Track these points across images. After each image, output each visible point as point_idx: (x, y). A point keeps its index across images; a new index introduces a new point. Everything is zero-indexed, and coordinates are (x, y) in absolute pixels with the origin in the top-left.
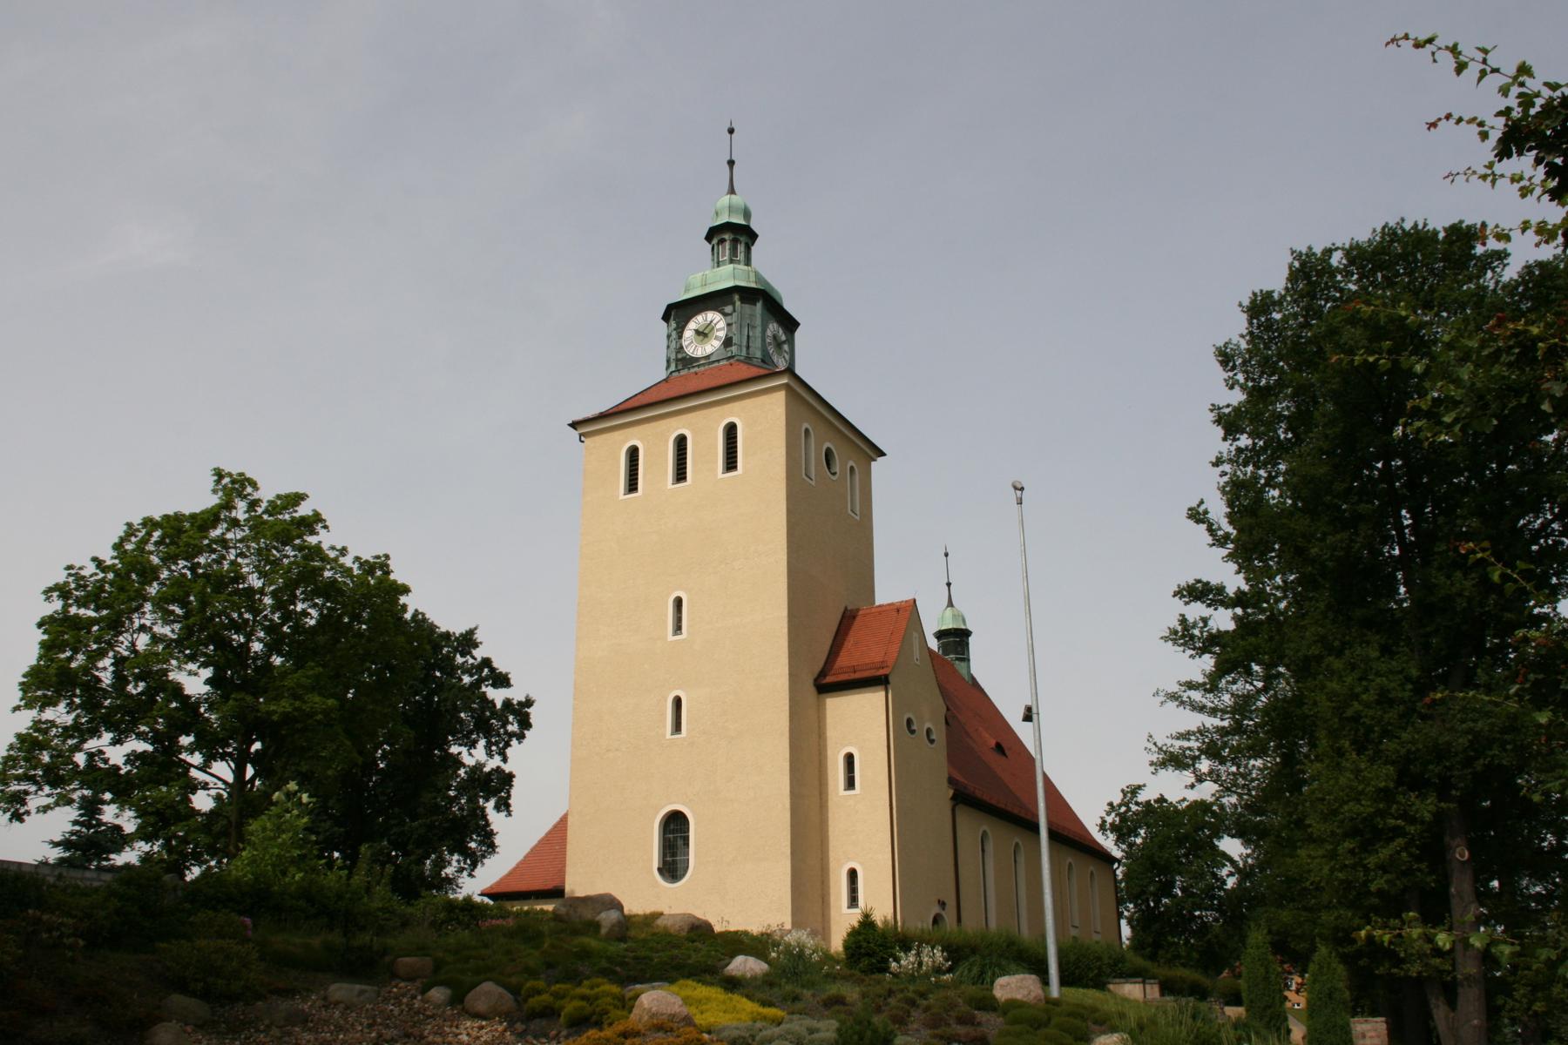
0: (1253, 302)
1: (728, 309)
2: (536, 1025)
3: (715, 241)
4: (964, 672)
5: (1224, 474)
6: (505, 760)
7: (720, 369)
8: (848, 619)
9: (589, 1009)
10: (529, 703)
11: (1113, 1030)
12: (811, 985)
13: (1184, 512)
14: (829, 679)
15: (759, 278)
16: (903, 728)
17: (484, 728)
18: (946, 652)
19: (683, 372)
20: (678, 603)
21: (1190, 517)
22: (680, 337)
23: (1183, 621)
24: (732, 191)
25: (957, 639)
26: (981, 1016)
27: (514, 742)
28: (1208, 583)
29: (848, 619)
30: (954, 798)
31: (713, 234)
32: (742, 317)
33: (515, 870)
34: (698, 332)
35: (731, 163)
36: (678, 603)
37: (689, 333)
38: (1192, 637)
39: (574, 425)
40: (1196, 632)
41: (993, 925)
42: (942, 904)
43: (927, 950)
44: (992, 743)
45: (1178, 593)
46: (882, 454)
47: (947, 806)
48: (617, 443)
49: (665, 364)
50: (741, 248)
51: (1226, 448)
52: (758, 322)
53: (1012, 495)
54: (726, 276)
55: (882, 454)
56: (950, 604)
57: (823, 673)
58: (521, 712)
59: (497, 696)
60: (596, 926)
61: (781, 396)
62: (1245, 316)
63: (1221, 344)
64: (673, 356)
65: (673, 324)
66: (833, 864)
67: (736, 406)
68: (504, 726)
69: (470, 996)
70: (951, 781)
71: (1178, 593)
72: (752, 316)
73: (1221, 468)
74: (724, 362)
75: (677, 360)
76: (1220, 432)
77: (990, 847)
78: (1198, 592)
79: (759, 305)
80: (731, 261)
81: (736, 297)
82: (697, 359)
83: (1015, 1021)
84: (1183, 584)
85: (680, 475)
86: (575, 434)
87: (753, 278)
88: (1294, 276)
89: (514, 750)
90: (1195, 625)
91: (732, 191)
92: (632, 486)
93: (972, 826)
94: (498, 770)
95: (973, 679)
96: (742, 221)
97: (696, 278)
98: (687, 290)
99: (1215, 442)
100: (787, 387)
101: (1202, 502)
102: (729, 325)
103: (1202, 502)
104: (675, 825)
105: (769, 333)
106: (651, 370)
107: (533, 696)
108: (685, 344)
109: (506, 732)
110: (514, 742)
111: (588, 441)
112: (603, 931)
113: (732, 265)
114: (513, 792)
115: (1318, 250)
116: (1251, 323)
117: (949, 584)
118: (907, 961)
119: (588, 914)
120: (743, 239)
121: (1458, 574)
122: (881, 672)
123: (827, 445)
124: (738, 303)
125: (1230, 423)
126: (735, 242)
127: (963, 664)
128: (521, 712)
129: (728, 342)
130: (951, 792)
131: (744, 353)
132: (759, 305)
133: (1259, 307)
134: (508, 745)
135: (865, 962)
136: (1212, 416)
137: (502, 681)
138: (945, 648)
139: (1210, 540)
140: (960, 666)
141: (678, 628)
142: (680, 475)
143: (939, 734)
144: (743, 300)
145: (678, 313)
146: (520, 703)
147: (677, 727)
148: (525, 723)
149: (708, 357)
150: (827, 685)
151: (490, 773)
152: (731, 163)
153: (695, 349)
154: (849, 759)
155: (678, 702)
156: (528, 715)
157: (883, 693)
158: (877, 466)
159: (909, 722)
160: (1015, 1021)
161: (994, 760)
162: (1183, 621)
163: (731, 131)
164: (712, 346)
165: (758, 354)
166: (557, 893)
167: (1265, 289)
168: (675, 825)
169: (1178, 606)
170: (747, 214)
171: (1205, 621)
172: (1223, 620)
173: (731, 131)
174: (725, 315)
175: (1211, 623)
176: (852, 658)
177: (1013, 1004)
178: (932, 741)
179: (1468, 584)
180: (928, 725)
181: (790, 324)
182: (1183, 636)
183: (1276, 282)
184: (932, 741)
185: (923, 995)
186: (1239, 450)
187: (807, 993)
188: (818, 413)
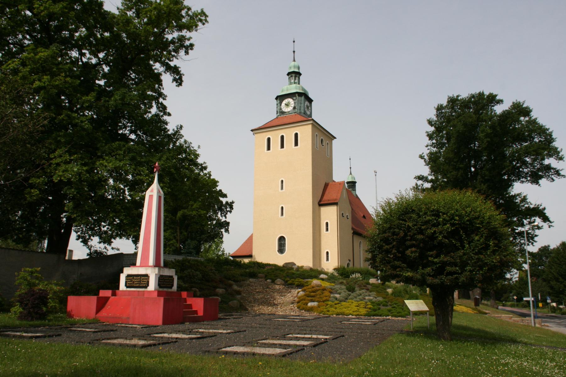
0: (438, 107)
1: (295, 98)
2: (289, 286)
3: (290, 76)
4: (354, 194)
5: (428, 149)
6: (226, 218)
7: (292, 116)
8: (326, 185)
9: (300, 283)
10: (233, 202)
11: (391, 288)
12: (336, 280)
13: (418, 156)
14: (322, 203)
15: (303, 89)
16: (341, 216)
17: (220, 209)
18: (349, 188)
19: (282, 116)
20: (282, 181)
21: (420, 157)
22: (281, 105)
23: (417, 184)
24: (294, 61)
25: (352, 184)
26: (368, 286)
27: (229, 213)
28: (423, 176)
29: (326, 185)
30: (353, 233)
31: (288, 74)
32: (298, 101)
33: (239, 248)
34: (286, 104)
35: (294, 52)
36: (282, 181)
37: (283, 104)
38: (419, 189)
39: (252, 130)
40: (420, 188)
41: (362, 266)
42: (350, 261)
43: (357, 274)
44: (362, 215)
45: (415, 178)
46: (335, 138)
47: (351, 235)
48: (264, 136)
49: (276, 112)
50: (297, 78)
51: (430, 142)
52: (303, 102)
53: (374, 174)
54: (293, 89)
55: (335, 138)
56: (351, 174)
57: (320, 201)
58: (230, 205)
59: (224, 200)
60: (293, 268)
61: (310, 126)
62: (435, 111)
63: (428, 119)
64: (279, 111)
65: (279, 102)
66: (322, 250)
67: (298, 128)
68: (226, 209)
69: (276, 281)
70: (353, 229)
71: (415, 178)
72: (301, 100)
73: (428, 148)
74: (294, 114)
75: (280, 112)
76: (428, 138)
77: (362, 245)
78: (420, 178)
79: (303, 97)
80: (295, 83)
81: (297, 95)
82: (286, 112)
83: (374, 286)
84: (417, 175)
85: (282, 146)
86: (252, 133)
87: (301, 89)
88: (448, 102)
89: (229, 215)
90: (419, 186)
91: (294, 61)
92: (269, 148)
93: (357, 240)
94: (225, 221)
95: (357, 195)
96: (298, 71)
97: (285, 88)
98: (282, 91)
99: (427, 141)
100: (312, 124)
101: (423, 153)
102: (295, 103)
103: (423, 153)
104: (282, 240)
105: (305, 105)
106: (273, 115)
107: (234, 201)
108: (282, 107)
109: (226, 210)
110: (229, 213)
111: (256, 135)
112: (294, 269)
113: (295, 85)
114: (229, 227)
115: (455, 96)
116: (437, 112)
117: (350, 168)
118: (354, 276)
119: (290, 266)
120: (298, 76)
121: (482, 184)
122: (336, 201)
123: (322, 138)
124: (297, 97)
125: (430, 137)
126: (295, 77)
127: (354, 191)
128: (230, 205)
129: (294, 108)
130: (352, 232)
131: (299, 111)
132: (303, 97)
133: (439, 108)
134: (226, 214)
135: (344, 276)
136: (426, 134)
137: (225, 196)
138: (349, 187)
139: (425, 164)
140: (353, 192)
141: (282, 188)
142: (282, 146)
143: (350, 217)
144: (299, 96)
145: (280, 98)
146: (230, 202)
147: (282, 214)
148: (231, 208)
149: (289, 112)
150: (321, 205)
151: (223, 222)
152: (294, 52)
153: (285, 109)
154: (327, 224)
155: (282, 208)
156: (233, 206)
157: (336, 207)
158: (334, 142)
159: (343, 214)
160: (374, 286)
161: (363, 220)
162: (417, 184)
163: (294, 42)
164: (290, 109)
165: (303, 112)
166: (250, 256)
167: (441, 103)
168: (282, 240)
169: (415, 181)
170: (299, 68)
171: (422, 185)
172: (428, 185)
173: (294, 42)
174: (294, 100)
175: (424, 185)
176: (329, 196)
177: (373, 284)
178: (348, 218)
179: (484, 187)
180: (347, 214)
181: (310, 101)
182: (416, 189)
183: (445, 103)
184: (348, 218)
185: (357, 282)
186: (433, 143)
187: (336, 281)
188: (320, 130)
